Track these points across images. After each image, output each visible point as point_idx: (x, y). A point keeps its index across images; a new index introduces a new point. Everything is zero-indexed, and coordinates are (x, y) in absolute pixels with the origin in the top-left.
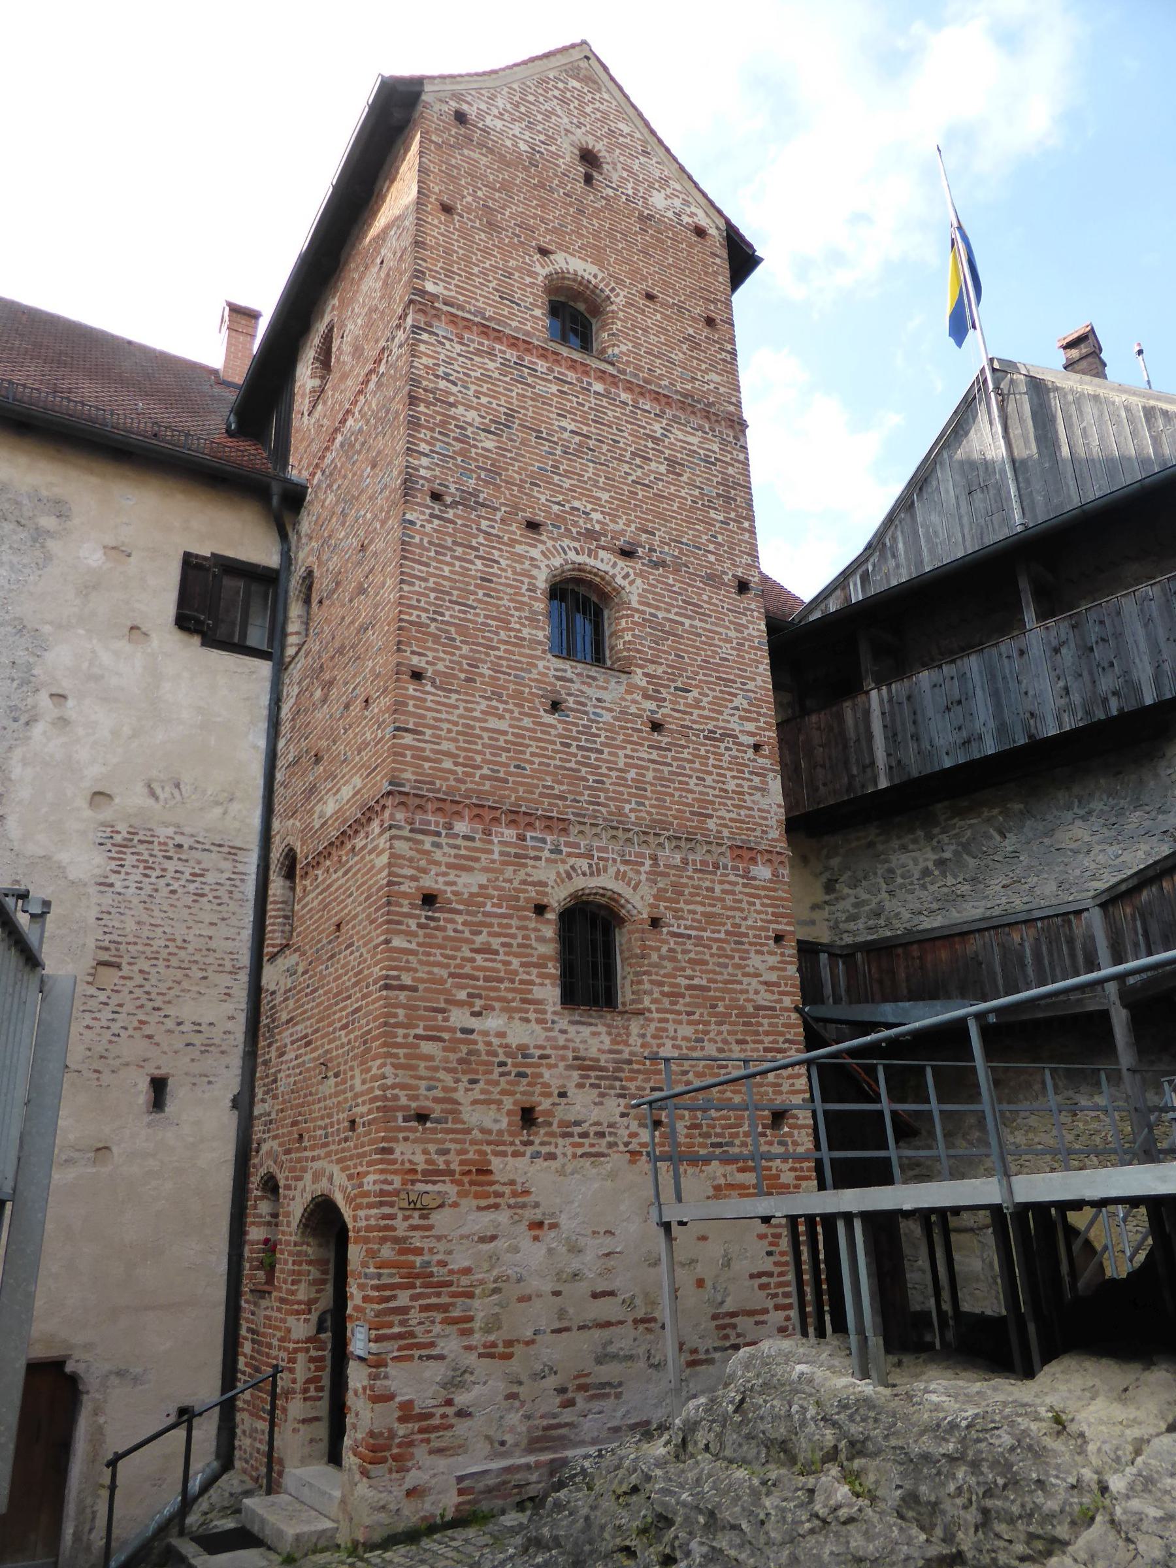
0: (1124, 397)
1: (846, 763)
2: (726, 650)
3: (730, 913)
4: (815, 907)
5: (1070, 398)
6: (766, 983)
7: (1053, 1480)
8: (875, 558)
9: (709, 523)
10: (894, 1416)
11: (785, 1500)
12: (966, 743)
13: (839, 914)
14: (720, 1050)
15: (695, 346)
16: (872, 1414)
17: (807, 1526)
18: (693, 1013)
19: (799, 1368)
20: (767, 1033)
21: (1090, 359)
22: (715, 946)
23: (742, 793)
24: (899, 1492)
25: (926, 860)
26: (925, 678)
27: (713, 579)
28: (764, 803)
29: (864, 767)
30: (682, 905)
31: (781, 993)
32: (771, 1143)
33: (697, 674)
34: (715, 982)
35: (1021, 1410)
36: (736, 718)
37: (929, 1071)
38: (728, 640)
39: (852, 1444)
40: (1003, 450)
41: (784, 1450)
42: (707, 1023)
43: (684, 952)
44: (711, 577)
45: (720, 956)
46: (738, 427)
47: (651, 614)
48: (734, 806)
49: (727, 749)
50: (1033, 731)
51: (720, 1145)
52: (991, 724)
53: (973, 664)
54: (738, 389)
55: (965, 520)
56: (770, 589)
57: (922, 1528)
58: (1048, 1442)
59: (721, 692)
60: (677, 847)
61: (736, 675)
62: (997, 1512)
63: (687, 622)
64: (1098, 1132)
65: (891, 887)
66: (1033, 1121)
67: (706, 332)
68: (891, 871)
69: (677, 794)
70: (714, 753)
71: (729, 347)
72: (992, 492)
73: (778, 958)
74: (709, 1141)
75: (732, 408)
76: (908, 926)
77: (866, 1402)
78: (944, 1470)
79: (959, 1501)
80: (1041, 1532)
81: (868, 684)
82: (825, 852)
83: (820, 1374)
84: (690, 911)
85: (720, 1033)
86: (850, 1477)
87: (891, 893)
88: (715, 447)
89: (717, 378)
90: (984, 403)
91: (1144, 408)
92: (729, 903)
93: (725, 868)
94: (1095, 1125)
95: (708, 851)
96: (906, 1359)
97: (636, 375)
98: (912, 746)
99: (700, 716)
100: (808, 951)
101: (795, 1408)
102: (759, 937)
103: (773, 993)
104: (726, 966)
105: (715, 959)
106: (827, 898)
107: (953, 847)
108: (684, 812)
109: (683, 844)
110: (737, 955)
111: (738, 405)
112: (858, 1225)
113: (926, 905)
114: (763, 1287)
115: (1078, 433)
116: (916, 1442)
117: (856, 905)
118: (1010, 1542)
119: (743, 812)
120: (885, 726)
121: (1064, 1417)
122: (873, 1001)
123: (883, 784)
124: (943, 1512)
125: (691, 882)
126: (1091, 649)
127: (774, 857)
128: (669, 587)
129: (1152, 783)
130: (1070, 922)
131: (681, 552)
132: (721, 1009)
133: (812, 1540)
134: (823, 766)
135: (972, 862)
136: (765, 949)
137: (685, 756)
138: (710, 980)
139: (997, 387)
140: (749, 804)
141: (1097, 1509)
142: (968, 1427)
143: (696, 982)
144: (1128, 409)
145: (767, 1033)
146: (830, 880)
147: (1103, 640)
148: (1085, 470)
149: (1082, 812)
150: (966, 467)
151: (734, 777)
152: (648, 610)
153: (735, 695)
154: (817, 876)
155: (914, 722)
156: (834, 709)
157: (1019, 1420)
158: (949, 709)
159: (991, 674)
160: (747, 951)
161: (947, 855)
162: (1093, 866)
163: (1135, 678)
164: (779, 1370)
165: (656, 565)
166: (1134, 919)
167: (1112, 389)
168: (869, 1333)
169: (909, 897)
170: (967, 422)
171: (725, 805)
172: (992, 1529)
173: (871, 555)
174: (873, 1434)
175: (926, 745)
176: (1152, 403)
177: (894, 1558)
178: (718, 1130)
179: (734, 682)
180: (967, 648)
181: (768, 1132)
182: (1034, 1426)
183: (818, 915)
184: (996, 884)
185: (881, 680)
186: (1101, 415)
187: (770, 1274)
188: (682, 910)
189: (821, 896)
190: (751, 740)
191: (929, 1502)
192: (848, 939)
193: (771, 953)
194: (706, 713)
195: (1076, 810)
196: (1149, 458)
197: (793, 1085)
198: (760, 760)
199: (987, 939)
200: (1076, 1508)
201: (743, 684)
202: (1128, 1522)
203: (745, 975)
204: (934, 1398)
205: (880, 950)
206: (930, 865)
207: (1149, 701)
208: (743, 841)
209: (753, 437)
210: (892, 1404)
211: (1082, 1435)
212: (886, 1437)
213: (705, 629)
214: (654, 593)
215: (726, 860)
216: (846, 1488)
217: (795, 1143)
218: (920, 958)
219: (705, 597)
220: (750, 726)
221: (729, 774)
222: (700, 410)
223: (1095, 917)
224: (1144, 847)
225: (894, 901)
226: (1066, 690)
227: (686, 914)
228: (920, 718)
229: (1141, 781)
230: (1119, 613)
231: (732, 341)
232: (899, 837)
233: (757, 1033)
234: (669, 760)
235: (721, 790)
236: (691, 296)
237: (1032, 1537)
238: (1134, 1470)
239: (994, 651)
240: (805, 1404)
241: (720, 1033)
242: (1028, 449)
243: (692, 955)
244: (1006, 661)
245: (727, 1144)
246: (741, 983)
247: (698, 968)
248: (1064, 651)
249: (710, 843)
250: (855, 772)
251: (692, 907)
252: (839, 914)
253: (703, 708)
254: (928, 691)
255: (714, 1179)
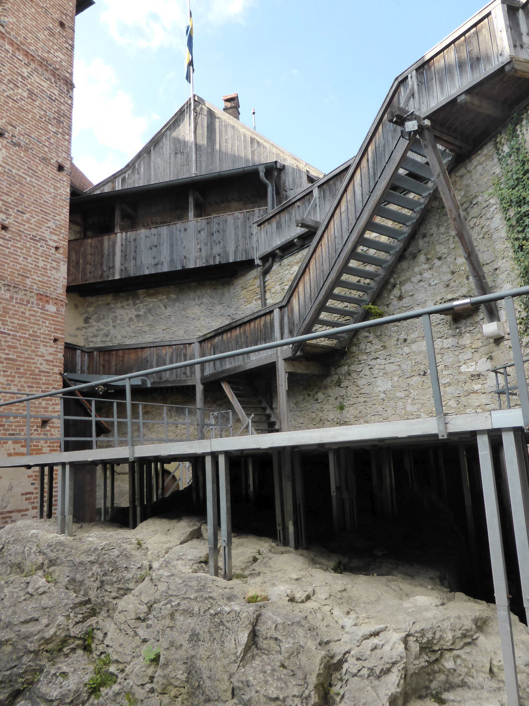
0: (244, 130)
1: (102, 264)
2: (47, 197)
3: (32, 325)
4: (78, 329)
5: (223, 124)
6: (47, 360)
7: (132, 566)
8: (130, 172)
9: (47, 131)
10: (72, 548)
11: (15, 588)
12: (156, 265)
13: (89, 334)
14: (19, 390)
15: (52, 34)
16: (62, 548)
17: (24, 597)
18: (7, 371)
19: (32, 531)
20: (44, 384)
21: (234, 109)
22: (22, 340)
23: (46, 269)
24: (68, 578)
25: (132, 314)
26: (143, 232)
27: (45, 160)
28: (57, 275)
29: (110, 268)
30: (7, 319)
31: (53, 366)
32: (40, 434)
33: (31, 206)
34: (20, 357)
35: (125, 541)
36: (48, 232)
37: (115, 405)
38: (50, 193)
39: (51, 561)
40: (192, 139)
41: (19, 567)
42: (14, 377)
43: (5, 341)
44: (44, 159)
45: (24, 345)
46: (69, 86)
47: (9, 170)
48: (41, 274)
49: (41, 246)
50: (185, 265)
51: (14, 434)
52: (168, 259)
53: (164, 230)
54: (72, 67)
55: (172, 165)
56: (75, 172)
57: (75, 592)
58: (133, 552)
59: (42, 217)
60: (8, 290)
61: (51, 211)
62: (107, 581)
63: (28, 179)
64: (184, 434)
65: (114, 324)
66: (160, 429)
67: (59, 29)
68: (115, 317)
69: (11, 264)
70: (34, 247)
71: (71, 42)
72: (185, 156)
73: (54, 349)
74: (8, 433)
75: (68, 75)
76: (120, 342)
77: (61, 543)
78: (88, 568)
79: (92, 579)
80: (123, 587)
81: (117, 230)
82: (86, 304)
83: (41, 533)
84: (11, 322)
85: (20, 382)
86: (46, 575)
87: (114, 327)
88: (56, 92)
89: (62, 57)
90: (188, 114)
91: (251, 137)
92: (32, 321)
93: (33, 303)
94: (184, 431)
95: (25, 294)
96: (84, 525)
97: (16, 38)
98: (133, 262)
99: (29, 227)
100: (70, 348)
101: (27, 548)
102: (46, 338)
103: (49, 365)
104: (27, 350)
105: (22, 347)
106: (85, 325)
107: (144, 310)
108: (14, 273)
109: (11, 289)
110: (33, 346)
111: (71, 74)
112: (67, 467)
113: (129, 334)
114: (27, 499)
115: (224, 140)
116: (78, 557)
117: (97, 330)
118: (110, 592)
119: (46, 278)
120: (122, 251)
121: (142, 542)
122: (99, 374)
123: (117, 277)
124: (85, 584)
125: (13, 308)
126: (213, 234)
127: (58, 302)
128: (21, 159)
129: (227, 295)
130: (186, 347)
131: (30, 141)
132: (22, 370)
133: (24, 603)
134: (90, 264)
135: (151, 318)
136: (48, 344)
137: (18, 245)
138: (17, 357)
139: (195, 109)
140: (49, 275)
141: (147, 575)
142: (102, 549)
143: (11, 356)
144: (244, 136)
145: (44, 384)
146: (87, 317)
147: (218, 231)
148: (224, 157)
149: (199, 303)
150: (176, 141)
151: (43, 261)
152: (7, 167)
153: (49, 221)
154: (81, 314)
155: (135, 252)
156: (99, 238)
157: (123, 544)
158: (151, 248)
159: (171, 236)
160: (39, 345)
161: (141, 313)
162: (199, 326)
163: (228, 249)
164: (23, 533)
165: (15, 144)
166: (211, 349)
167: (240, 125)
168: (67, 513)
169: (122, 330)
170: (180, 120)
171: (37, 273)
172: (104, 589)
173: (128, 170)
174: (60, 556)
175: (139, 263)
176: (254, 136)
177: (60, 605)
178: (13, 428)
179: (50, 214)
180: (163, 223)
181: (39, 429)
182: (128, 547)
183: (79, 333)
184: (159, 329)
185: (123, 229)
186: (234, 135)
187: (32, 493)
188: (7, 321)
189: (81, 324)
190: (55, 245)
191: (79, 581)
192: (92, 345)
193: (51, 347)
194: (33, 226)
195: (197, 301)
196: (249, 160)
197: (54, 408)
198: (58, 255)
199: (152, 352)
200: (139, 576)
201: (54, 216)
202: (156, 578)
203: (36, 356)
204: (90, 539)
205: (105, 351)
206: (133, 317)
207: (231, 261)
208: (44, 292)
209: (76, 93)
210: (72, 543)
211: (147, 548)
212: (66, 557)
213: (37, 184)
214: (12, 159)
215: (34, 300)
216: (44, 580)
217: (51, 435)
218: (122, 357)
219: (40, 168)
220: (55, 238)
221: (41, 258)
222: (51, 70)
223: (197, 345)
224: (220, 321)
225: (115, 330)
226: (200, 249)
227: (9, 323)
228: (138, 250)
229: (223, 294)
230: (226, 222)
231: (72, 39)
232: (121, 302)
233: (38, 383)
234: (9, 246)
235: (35, 265)
236: (53, 6)
237: (120, 589)
238: (163, 559)
239: (174, 226)
240: (32, 546)
241: (20, 382)
242: (203, 141)
243: (10, 344)
244: (178, 232)
245: (17, 434)
246: (34, 359)
247: (12, 350)
248: (202, 232)
249: (26, 290)
250: (105, 269)
251: (12, 320)
252: (89, 334)
253: (31, 224)
254: (144, 239)
255: (9, 450)
